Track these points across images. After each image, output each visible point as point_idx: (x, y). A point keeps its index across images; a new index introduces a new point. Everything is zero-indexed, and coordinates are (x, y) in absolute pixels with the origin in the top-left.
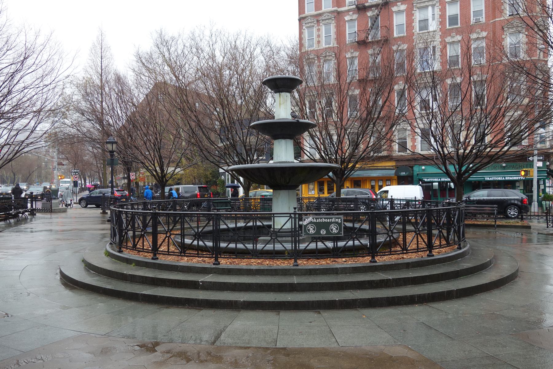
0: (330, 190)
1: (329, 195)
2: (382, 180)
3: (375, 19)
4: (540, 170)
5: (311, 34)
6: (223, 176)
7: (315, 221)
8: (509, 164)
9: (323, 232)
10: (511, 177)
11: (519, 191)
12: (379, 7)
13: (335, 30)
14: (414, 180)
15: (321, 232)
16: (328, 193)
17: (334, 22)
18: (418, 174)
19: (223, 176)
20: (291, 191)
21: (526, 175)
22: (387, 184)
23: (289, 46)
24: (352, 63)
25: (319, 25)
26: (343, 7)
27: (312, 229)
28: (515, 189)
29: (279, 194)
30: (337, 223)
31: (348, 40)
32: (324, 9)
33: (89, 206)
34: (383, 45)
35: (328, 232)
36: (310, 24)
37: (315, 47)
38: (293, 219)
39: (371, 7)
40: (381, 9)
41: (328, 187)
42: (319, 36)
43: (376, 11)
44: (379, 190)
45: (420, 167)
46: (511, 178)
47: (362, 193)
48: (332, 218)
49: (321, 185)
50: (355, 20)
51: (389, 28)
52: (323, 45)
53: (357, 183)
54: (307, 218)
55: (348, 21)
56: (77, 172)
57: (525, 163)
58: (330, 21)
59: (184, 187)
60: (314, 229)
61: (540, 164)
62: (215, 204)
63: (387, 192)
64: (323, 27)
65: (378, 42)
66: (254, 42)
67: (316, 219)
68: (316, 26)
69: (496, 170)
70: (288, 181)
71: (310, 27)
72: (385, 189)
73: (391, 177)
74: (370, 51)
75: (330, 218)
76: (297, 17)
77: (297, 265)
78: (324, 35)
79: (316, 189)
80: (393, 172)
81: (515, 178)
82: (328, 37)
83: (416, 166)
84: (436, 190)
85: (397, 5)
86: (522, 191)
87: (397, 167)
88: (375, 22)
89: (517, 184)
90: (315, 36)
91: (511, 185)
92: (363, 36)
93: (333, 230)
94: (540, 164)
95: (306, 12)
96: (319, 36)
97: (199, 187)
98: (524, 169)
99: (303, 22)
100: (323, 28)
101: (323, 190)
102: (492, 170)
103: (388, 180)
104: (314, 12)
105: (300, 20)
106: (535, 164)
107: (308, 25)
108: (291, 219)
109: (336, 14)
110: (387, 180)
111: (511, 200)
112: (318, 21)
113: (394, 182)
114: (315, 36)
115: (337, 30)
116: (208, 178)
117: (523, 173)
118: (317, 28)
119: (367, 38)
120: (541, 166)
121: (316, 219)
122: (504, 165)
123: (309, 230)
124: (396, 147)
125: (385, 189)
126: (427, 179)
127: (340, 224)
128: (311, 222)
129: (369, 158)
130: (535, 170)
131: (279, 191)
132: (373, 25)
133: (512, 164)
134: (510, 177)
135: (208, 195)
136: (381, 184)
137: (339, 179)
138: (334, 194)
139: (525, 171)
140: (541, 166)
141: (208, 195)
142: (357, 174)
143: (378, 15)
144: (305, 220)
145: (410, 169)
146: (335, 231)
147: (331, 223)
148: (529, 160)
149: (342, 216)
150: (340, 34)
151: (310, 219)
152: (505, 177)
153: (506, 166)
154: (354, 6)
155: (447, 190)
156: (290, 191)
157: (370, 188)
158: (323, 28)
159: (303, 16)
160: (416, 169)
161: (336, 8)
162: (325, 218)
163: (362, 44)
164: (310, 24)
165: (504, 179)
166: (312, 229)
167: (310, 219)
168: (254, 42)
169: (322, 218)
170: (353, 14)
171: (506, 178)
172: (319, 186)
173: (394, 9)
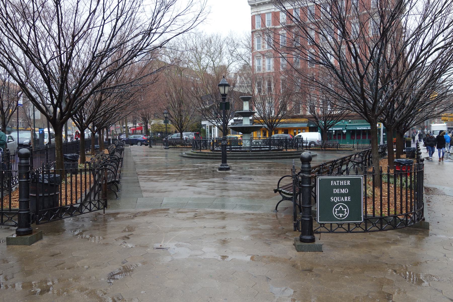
5: (259, 41)
9: (341, 211)
35: (259, 144)
63: (300, 136)
66: (222, 39)
76: (250, 29)
80: (306, 124)
102: (362, 123)
103: (303, 129)
105: (252, 32)
113: (307, 130)
122: (350, 121)
138: (267, 136)
146: (260, 144)
151: (254, 141)
163: (289, 49)
167: (254, 141)
168: (222, 39)
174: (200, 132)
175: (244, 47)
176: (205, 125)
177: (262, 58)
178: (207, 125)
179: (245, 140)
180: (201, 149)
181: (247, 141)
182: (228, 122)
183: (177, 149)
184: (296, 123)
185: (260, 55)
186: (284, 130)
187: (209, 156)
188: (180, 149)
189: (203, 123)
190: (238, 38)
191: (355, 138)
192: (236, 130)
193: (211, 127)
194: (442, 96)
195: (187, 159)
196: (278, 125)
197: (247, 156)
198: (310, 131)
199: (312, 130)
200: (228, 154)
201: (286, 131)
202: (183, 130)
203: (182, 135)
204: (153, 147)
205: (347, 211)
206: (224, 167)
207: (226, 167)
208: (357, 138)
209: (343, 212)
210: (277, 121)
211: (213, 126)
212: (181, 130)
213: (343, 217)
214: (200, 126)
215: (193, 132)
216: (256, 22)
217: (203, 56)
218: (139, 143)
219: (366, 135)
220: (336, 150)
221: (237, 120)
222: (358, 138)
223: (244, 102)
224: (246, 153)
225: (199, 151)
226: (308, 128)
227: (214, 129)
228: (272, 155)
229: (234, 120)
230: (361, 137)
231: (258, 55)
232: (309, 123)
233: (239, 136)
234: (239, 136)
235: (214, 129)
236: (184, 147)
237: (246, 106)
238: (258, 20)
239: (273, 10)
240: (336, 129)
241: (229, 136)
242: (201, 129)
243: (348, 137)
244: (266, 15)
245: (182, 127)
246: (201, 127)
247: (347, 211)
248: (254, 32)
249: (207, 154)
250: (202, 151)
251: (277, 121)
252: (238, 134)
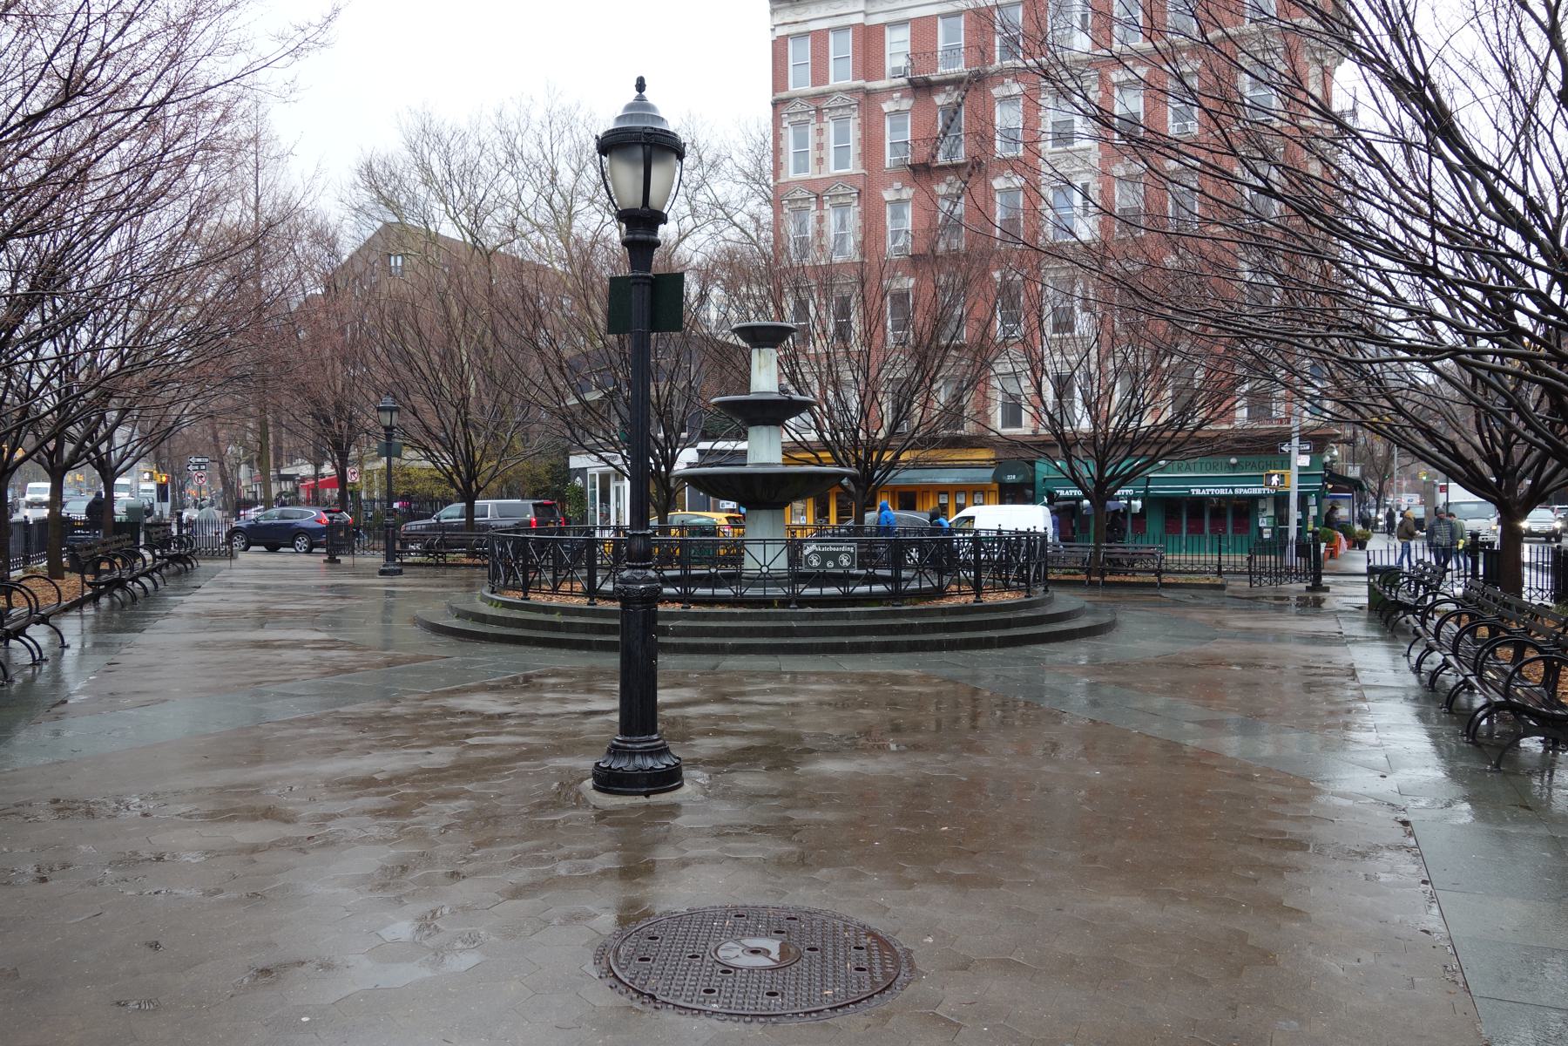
2: (946, 493)
3: (952, 113)
4: (1304, 474)
5: (801, 142)
6: (578, 479)
8: (1245, 459)
12: (962, 86)
13: (859, 134)
17: (856, 114)
19: (578, 479)
23: (743, 146)
24: (897, 215)
25: (820, 120)
26: (880, 79)
30: (849, 552)
31: (889, 159)
32: (832, 84)
33: (252, 548)
34: (970, 175)
36: (799, 117)
37: (812, 173)
39: (942, 84)
40: (967, 91)
41: (838, 508)
42: (820, 146)
43: (956, 94)
44: (957, 512)
46: (1246, 492)
50: (906, 111)
51: (984, 137)
52: (831, 170)
55: (890, 114)
56: (204, 464)
58: (847, 111)
61: (1305, 461)
63: (971, 519)
64: (832, 124)
65: (956, 168)
68: (813, 121)
69: (1217, 471)
71: (800, 123)
73: (985, 486)
74: (942, 189)
76: (767, 97)
78: (832, 145)
79: (810, 513)
80: (990, 473)
81: (1255, 491)
82: (842, 150)
84: (1088, 517)
85: (1003, 83)
87: (998, 462)
88: (952, 120)
89: (1261, 506)
90: (811, 147)
92: (924, 153)
94: (1305, 461)
95: (791, 87)
96: (820, 146)
99: (784, 110)
100: (831, 128)
102: (1208, 471)
103: (976, 492)
104: (809, 89)
105: (775, 104)
107: (793, 119)
109: (861, 96)
112: (818, 110)
113: (992, 497)
114: (811, 147)
115: (864, 134)
118: (817, 126)
119: (934, 157)
120: (1307, 464)
122: (1233, 460)
127: (852, 555)
128: (814, 552)
129: (933, 440)
132: (948, 128)
133: (1251, 459)
136: (963, 502)
140: (1307, 464)
142: (905, 477)
143: (959, 105)
145: (1028, 467)
147: (841, 552)
149: (855, 544)
150: (871, 147)
152: (1233, 489)
153: (1238, 464)
154: (903, 81)
155: (1129, 519)
158: (831, 128)
159: (784, 95)
161: (861, 83)
163: (922, 171)
164: (799, 117)
165: (1231, 492)
170: (902, 97)
171: (1237, 491)
173: (997, 92)
174: (563, 500)
175: (741, 178)
176: (582, 472)
177: (813, 208)
178: (590, 471)
179: (764, 542)
180: (526, 588)
181: (771, 550)
182: (674, 458)
183: (449, 571)
184: (954, 467)
185: (806, 196)
186: (900, 494)
187: (570, 627)
188: (464, 572)
189: (576, 462)
190: (715, 144)
191: (1225, 531)
192: (711, 486)
193: (605, 479)
195: (447, 639)
196: (893, 472)
197: (775, 632)
198: (1002, 502)
199: (1012, 494)
200: (671, 616)
201: (907, 499)
202: (479, 489)
203: (470, 511)
204: (345, 560)
206: (639, 761)
207: (650, 763)
208: (1190, 531)
210: (888, 456)
211: (617, 476)
212: (467, 485)
214: (564, 474)
215: (535, 496)
216: (791, 63)
217: (580, 205)
218: (302, 543)
219: (1225, 516)
220: (1151, 585)
221: (712, 452)
222: (1197, 529)
223: (755, 352)
224: (768, 617)
225: (515, 597)
226: (996, 485)
227: (617, 489)
228: (909, 629)
229: (701, 452)
230: (1207, 529)
231: (798, 195)
232: (1000, 465)
233: (719, 516)
234: (720, 518)
235: (617, 489)
236: (478, 561)
237: (764, 371)
238: (800, 54)
239: (858, 19)
241: (677, 516)
242: (565, 484)
243: (1155, 525)
244: (831, 36)
245: (472, 476)
246: (566, 480)
248: (785, 101)
249: (557, 618)
250: (537, 598)
251: (888, 456)
252: (717, 510)
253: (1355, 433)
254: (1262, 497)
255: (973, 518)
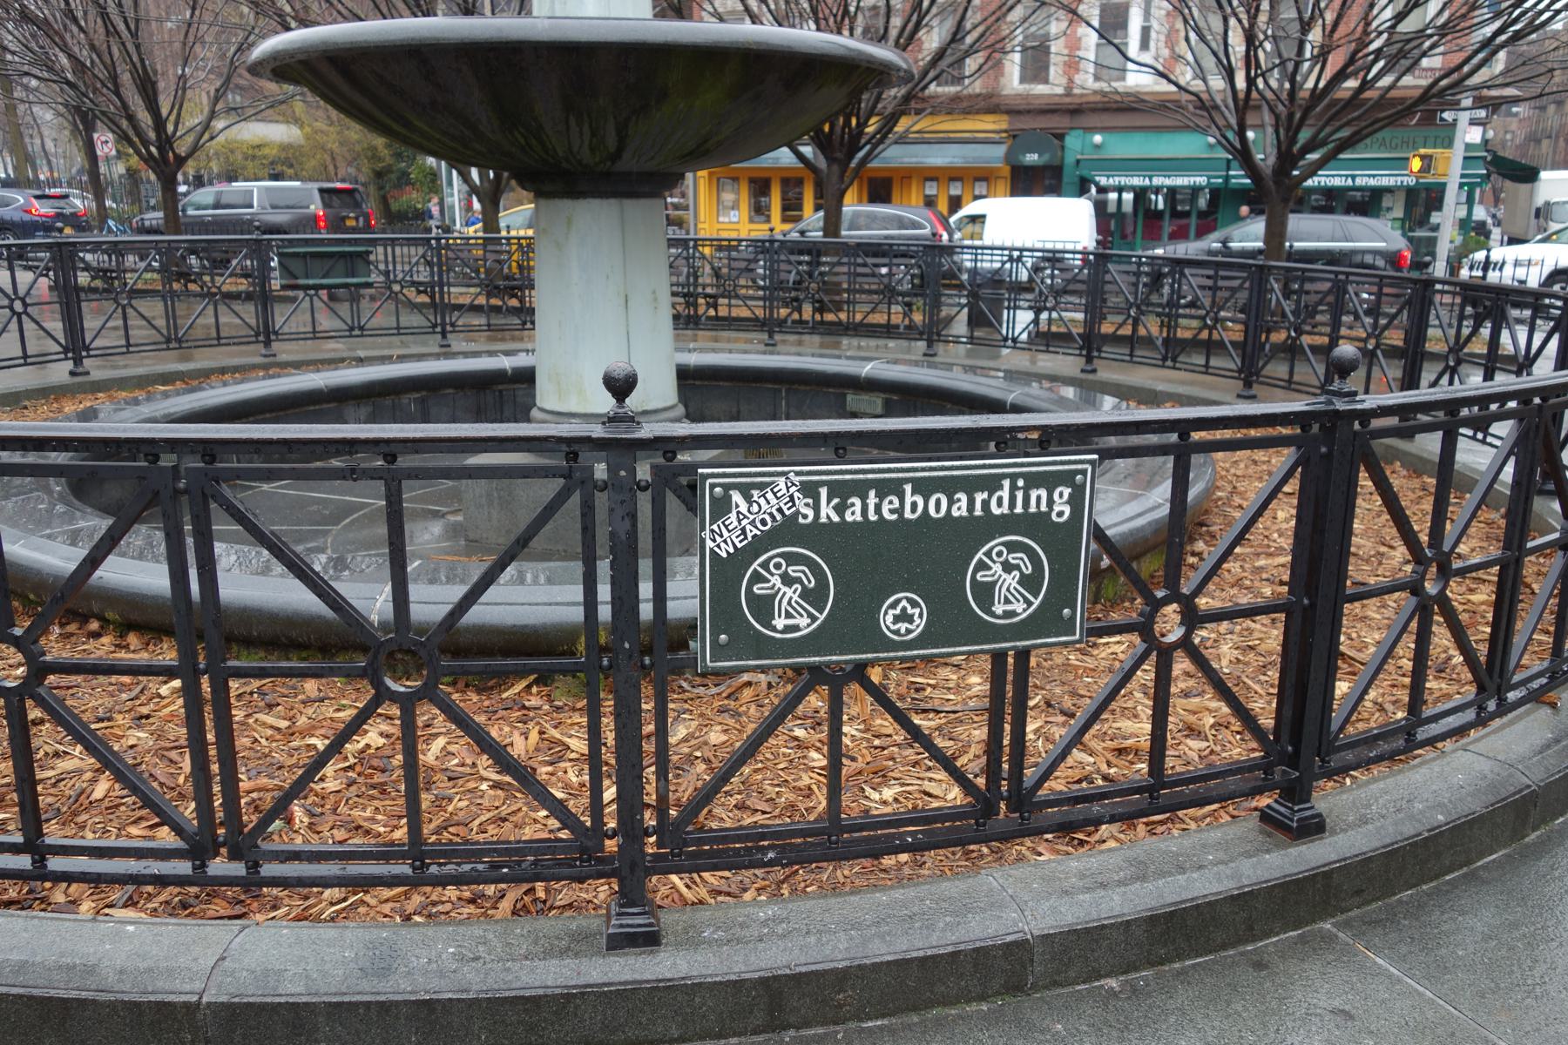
0: (791, 209)
1: (787, 227)
7: (827, 512)
9: (904, 617)
10: (1374, 176)
11: (1390, 224)
14: (1066, 179)
15: (887, 619)
16: (785, 220)
18: (1078, 162)
20: (634, 207)
21: (1425, 169)
22: (977, 193)
27: (791, 593)
28: (1377, 216)
29: (569, 222)
30: (1036, 524)
38: (602, 500)
41: (783, 199)
45: (1088, 136)
47: (902, 223)
48: (992, 484)
49: (760, 186)
53: (880, 191)
54: (746, 490)
57: (1431, 132)
59: (267, 189)
60: (814, 597)
62: (296, 266)
63: (977, 219)
67: (842, 492)
70: (611, 142)
72: (971, 209)
75: (970, 485)
77: (649, 940)
80: (1000, 151)
81: (1385, 182)
83: (1074, 133)
86: (1398, 224)
89: (1387, 201)
91: (1367, 203)
93: (1000, 593)
97: (321, 191)
98: (1422, 151)
101: (768, 208)
103: (979, 178)
106: (1459, 134)
108: (576, 499)
110: (977, 179)
111: (1364, 252)
116: (380, 159)
117: (1416, 164)
121: (842, 492)
123: (764, 608)
124: (1013, 64)
125: (971, 209)
126: (1108, 177)
128: (787, 531)
130: (1458, 153)
131: (566, 205)
134: (1369, 176)
135: (357, 219)
137: (835, 168)
139: (1423, 157)
141: (357, 219)
142: (894, 156)
144: (722, 507)
148: (1442, 119)
156: (630, 205)
157: (921, 203)
160: (1075, 144)
162: (924, 487)
165: (1350, 182)
166: (791, 593)
169: (893, 487)
171: (1359, 182)
172: (755, 197)
194: (165, 753)
199: (1027, 181)
205: (921, 616)
209: (910, 619)
213: (909, 632)
226: (1007, 171)
240: (1168, 182)
247: (888, 628)
253: (491, 223)
254: (1389, 190)
255: (984, 216)
